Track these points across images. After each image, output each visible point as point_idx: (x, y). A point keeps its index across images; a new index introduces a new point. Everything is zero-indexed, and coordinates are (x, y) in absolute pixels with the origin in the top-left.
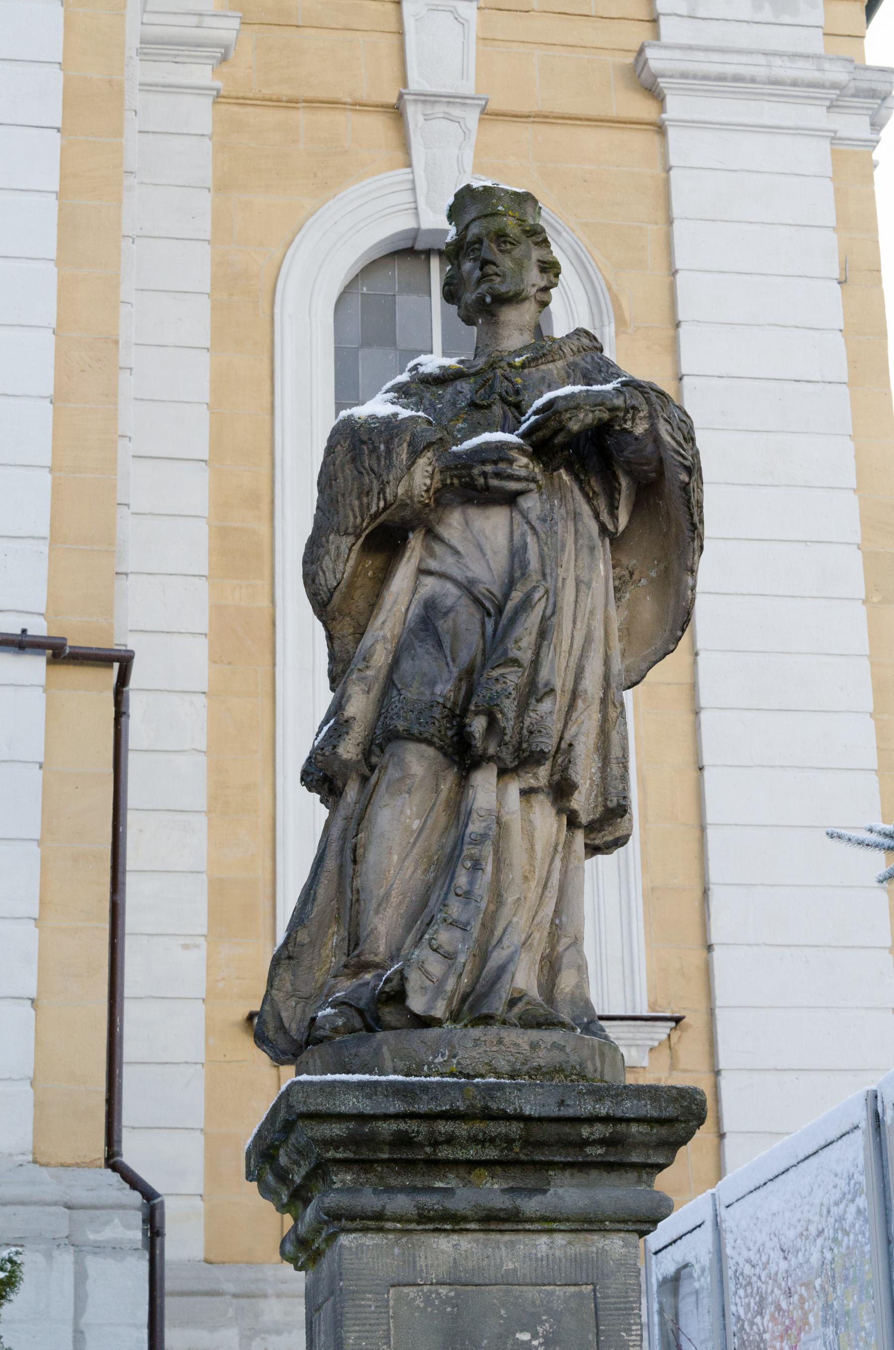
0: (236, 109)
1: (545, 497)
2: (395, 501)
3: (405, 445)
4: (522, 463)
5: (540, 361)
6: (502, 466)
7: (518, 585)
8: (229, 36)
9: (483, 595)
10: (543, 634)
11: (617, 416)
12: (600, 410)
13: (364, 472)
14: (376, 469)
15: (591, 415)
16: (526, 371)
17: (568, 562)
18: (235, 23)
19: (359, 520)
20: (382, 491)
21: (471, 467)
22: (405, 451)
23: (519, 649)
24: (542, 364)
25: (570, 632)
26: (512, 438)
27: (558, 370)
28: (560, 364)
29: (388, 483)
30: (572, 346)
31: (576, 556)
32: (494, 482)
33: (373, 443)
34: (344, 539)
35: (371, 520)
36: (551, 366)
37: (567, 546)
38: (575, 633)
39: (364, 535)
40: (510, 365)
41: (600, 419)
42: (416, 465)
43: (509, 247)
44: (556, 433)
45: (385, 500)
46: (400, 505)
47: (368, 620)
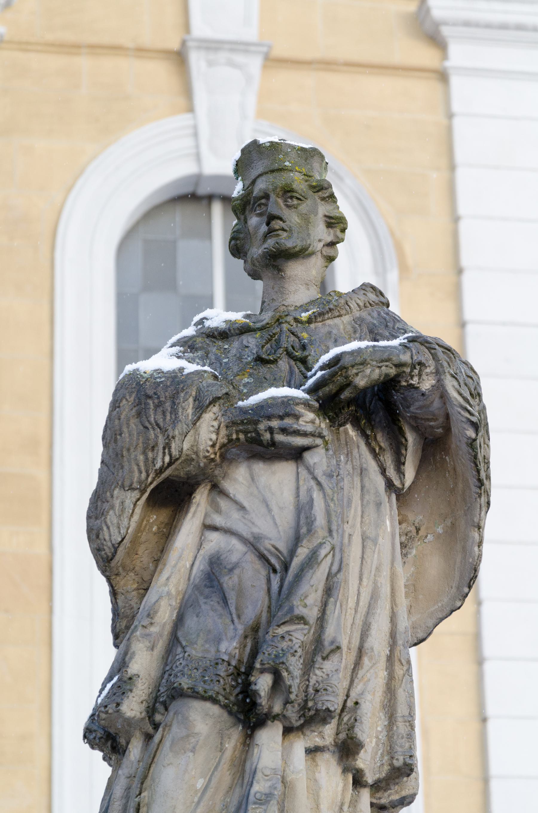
1: (331, 452)
3: (191, 400)
4: (309, 420)
5: (326, 316)
6: (288, 421)
9: (269, 551)
11: (404, 372)
12: (387, 366)
13: (150, 427)
14: (162, 424)
15: (377, 371)
16: (312, 326)
19: (144, 475)
20: (167, 446)
21: (257, 422)
22: (191, 406)
23: (305, 606)
24: (328, 319)
27: (344, 325)
28: (346, 319)
29: (173, 437)
31: (363, 512)
34: (129, 493)
37: (354, 502)
39: (149, 490)
40: (296, 320)
41: (387, 375)
42: (201, 420)
43: (295, 202)
44: (342, 389)
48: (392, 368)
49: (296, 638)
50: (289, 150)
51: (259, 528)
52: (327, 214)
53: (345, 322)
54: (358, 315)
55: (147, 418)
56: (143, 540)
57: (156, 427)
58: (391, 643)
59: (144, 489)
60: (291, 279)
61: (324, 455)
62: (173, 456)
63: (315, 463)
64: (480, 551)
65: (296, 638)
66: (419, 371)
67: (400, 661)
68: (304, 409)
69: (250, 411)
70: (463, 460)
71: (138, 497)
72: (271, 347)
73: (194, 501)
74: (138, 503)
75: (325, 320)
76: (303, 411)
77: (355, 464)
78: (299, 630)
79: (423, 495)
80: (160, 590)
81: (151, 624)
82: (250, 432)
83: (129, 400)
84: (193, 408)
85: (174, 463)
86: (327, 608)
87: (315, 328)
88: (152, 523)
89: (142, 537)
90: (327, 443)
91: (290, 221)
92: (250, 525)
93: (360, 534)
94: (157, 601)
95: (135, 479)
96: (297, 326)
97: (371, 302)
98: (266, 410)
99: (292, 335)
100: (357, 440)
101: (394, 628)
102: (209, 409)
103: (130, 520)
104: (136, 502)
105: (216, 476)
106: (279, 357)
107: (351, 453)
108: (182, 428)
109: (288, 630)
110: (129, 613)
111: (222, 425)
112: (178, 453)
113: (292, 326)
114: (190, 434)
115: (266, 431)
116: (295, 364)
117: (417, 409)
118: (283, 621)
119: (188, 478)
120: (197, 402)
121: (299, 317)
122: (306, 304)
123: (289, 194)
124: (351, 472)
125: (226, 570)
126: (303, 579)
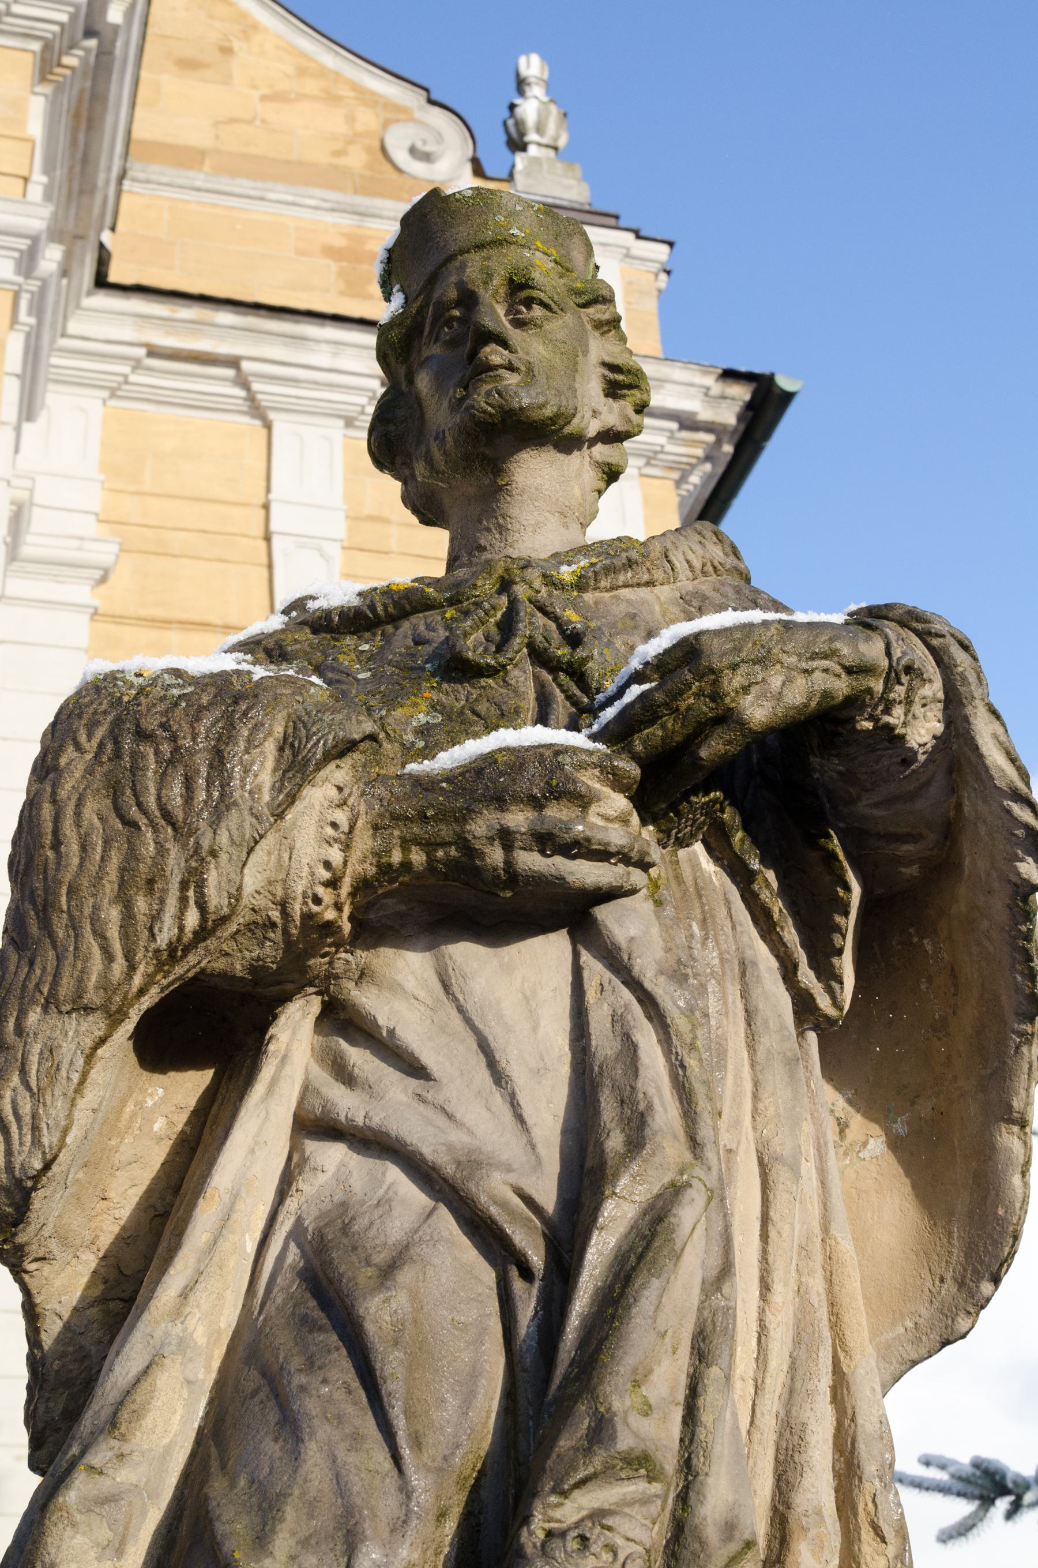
0: (113, 627)
1: (669, 911)
2: (233, 909)
3: (270, 747)
4: (610, 814)
5: (621, 578)
6: (557, 813)
7: (624, 1181)
8: (107, 560)
9: (504, 1205)
10: (703, 1349)
11: (869, 691)
12: (826, 671)
13: (143, 821)
14: (179, 815)
15: (801, 681)
16: (589, 597)
17: (737, 1096)
18: (115, 548)
19: (119, 966)
20: (193, 879)
21: (464, 816)
22: (270, 764)
23: (647, 1409)
24: (626, 586)
25: (754, 1315)
26: (578, 740)
27: (661, 604)
28: (664, 592)
29: (213, 853)
30: (691, 556)
31: (756, 1084)
32: (530, 861)
33: (174, 738)
34: (72, 1023)
35: (160, 966)
36: (643, 592)
37: (731, 1053)
38: (771, 1319)
39: (134, 1016)
40: (548, 580)
41: (826, 695)
42: (299, 806)
43: (537, 311)
44: (702, 730)
45: (202, 907)
46: (251, 927)
47: (148, 1260)
48: (838, 676)
49: (628, 1539)
50: (518, 208)
51: (470, 1132)
52: (608, 359)
53: (662, 598)
54: (690, 588)
55: (136, 796)
56: (122, 1159)
57: (163, 823)
58: (841, 1465)
59: (119, 1011)
60: (525, 497)
61: (653, 918)
62: (211, 908)
63: (632, 939)
64: (1026, 1185)
65: (628, 1539)
66: (907, 693)
67: (876, 1529)
68: (600, 781)
69: (444, 785)
70: (987, 944)
71: (101, 1033)
72: (487, 639)
73: (271, 1047)
74: (100, 1052)
75: (617, 588)
76: (597, 786)
77: (724, 947)
78: (631, 1504)
79: (854, 1036)
80: (158, 1333)
81: (121, 1456)
82: (444, 844)
83: (87, 746)
84: (275, 770)
85: (212, 932)
86: (700, 1402)
87: (596, 603)
88: (152, 1110)
89: (122, 1148)
90: (657, 887)
91: (527, 353)
92: (441, 1121)
93: (753, 1147)
94: (146, 1371)
95: (94, 978)
96: (550, 595)
97: (716, 564)
98: (490, 779)
99: (539, 615)
100: (723, 885)
101: (847, 1422)
102: (322, 773)
103: (73, 1104)
104: (95, 1049)
105: (337, 977)
106: (511, 660)
107: (713, 917)
108: (240, 827)
109: (596, 1505)
110: (75, 1373)
111: (360, 823)
112: (226, 901)
113: (538, 592)
114: (264, 844)
115: (491, 840)
116: (554, 680)
117: (877, 805)
118: (580, 1475)
119: (255, 983)
120: (288, 751)
121: (554, 573)
122: (567, 552)
123: (523, 294)
124: (718, 969)
125: (370, 1271)
126: (634, 1310)
